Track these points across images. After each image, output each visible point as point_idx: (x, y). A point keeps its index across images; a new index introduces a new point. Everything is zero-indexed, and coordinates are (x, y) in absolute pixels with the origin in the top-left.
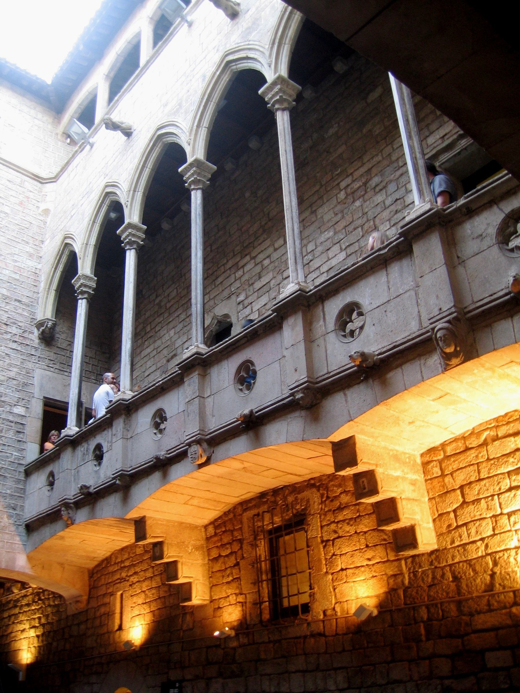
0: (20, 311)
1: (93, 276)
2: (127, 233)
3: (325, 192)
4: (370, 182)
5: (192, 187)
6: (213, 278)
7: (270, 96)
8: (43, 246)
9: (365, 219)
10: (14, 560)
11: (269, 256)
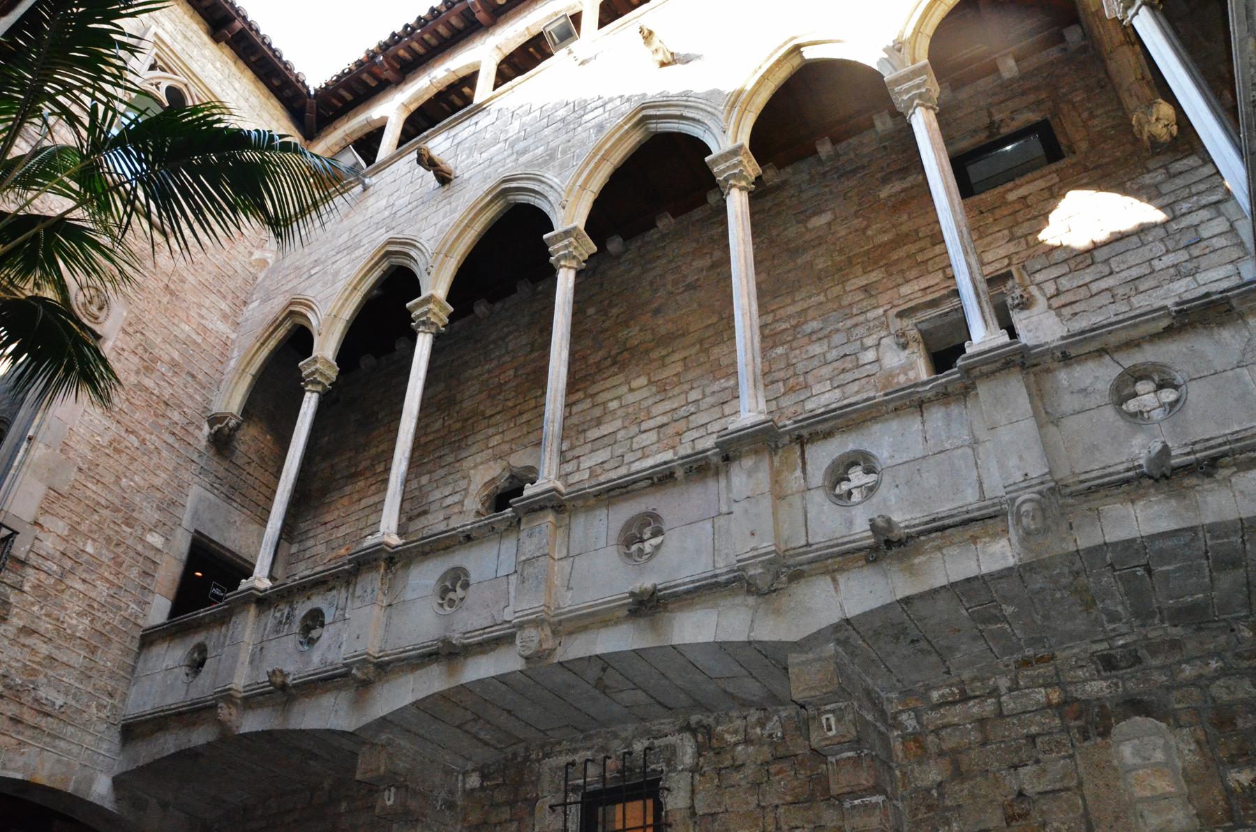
0: (191, 391)
2: (424, 309)
4: (804, 327)
5: (562, 263)
6: (516, 411)
7: (722, 167)
9: (790, 372)
10: (90, 781)
11: (619, 398)
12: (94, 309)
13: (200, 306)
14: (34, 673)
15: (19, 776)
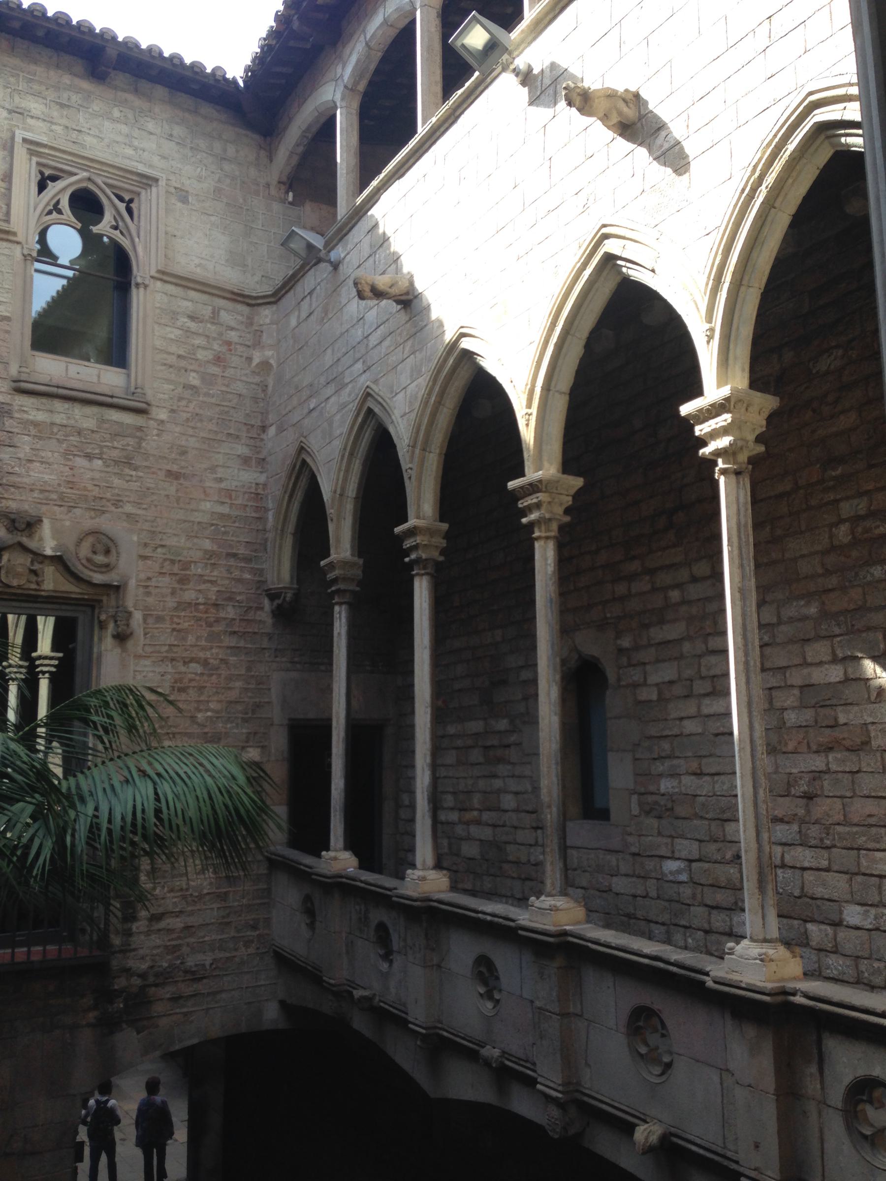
1: (356, 558)
3: (804, 506)
8: (264, 436)
12: (100, 559)
13: (213, 469)
14: (177, 947)
15: (195, 1041)
